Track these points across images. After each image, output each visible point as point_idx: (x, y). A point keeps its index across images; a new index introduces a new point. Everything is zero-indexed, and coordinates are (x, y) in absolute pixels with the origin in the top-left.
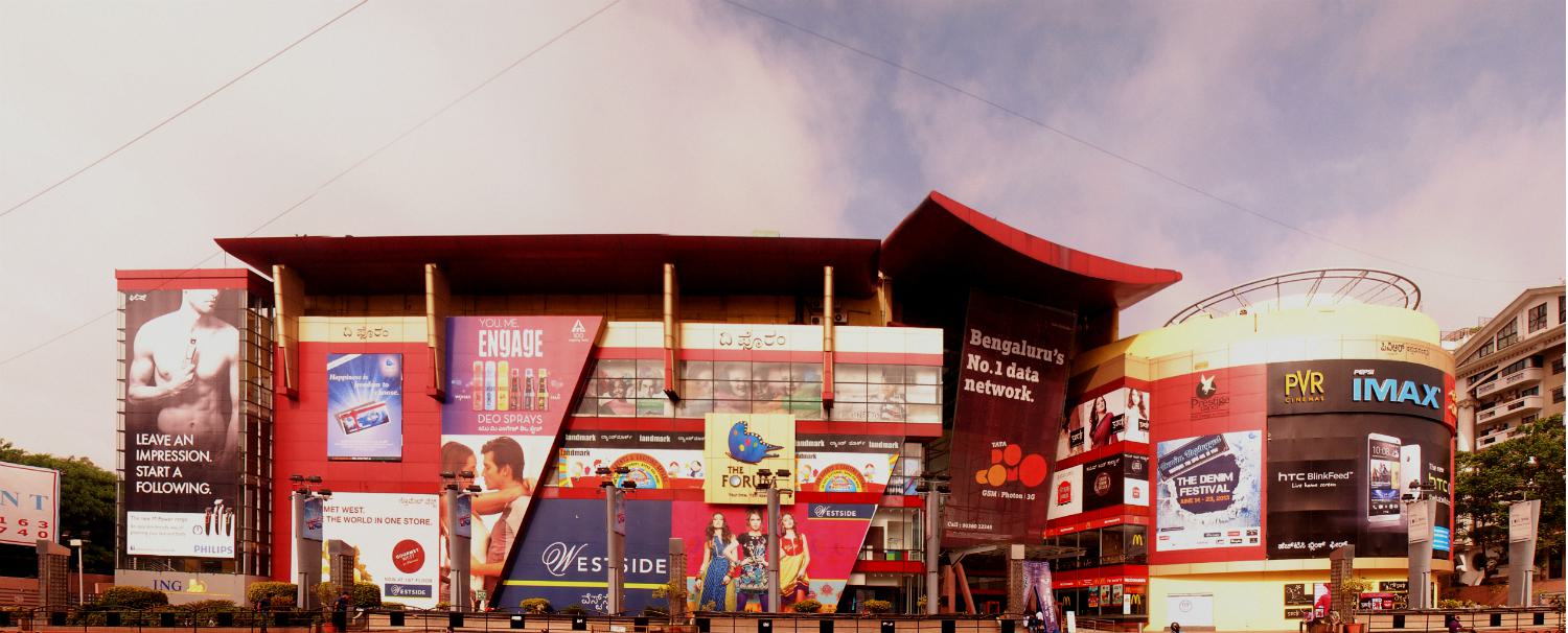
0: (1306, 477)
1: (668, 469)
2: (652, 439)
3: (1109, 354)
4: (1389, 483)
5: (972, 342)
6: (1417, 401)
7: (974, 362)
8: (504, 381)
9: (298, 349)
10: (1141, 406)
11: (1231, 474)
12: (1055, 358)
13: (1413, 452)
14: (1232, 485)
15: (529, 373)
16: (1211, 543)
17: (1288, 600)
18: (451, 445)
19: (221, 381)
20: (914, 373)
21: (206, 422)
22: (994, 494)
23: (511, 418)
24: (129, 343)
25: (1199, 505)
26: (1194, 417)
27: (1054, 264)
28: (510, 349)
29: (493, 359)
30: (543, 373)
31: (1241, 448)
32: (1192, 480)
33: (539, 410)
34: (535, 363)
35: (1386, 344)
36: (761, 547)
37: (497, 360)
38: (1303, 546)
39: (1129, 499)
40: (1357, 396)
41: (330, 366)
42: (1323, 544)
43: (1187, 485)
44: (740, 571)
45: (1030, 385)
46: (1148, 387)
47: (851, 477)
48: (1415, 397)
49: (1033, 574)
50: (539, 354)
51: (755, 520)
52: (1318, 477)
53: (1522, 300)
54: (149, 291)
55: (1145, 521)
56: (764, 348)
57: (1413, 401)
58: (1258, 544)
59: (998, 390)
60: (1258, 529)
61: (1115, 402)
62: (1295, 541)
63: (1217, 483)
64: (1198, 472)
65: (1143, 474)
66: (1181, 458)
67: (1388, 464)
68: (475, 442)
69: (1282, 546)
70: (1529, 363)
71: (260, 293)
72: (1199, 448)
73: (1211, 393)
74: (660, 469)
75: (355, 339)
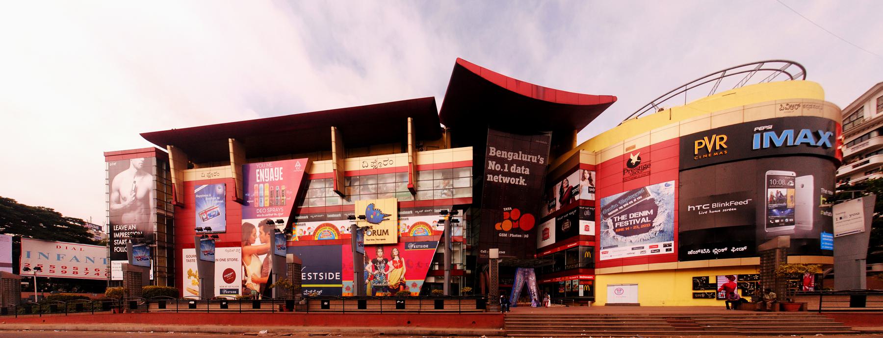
0: (710, 206)
1: (340, 230)
2: (333, 216)
3: (569, 155)
4: (784, 204)
5: (491, 154)
6: (813, 143)
7: (492, 165)
8: (267, 193)
9: (186, 186)
10: (590, 180)
11: (652, 211)
12: (538, 160)
13: (808, 181)
14: (652, 218)
15: (277, 188)
16: (638, 253)
17: (695, 286)
18: (247, 224)
19: (146, 199)
20: (458, 172)
21: (141, 219)
22: (506, 235)
23: (270, 210)
24: (110, 185)
25: (626, 232)
26: (624, 180)
27: (534, 97)
28: (273, 178)
29: (262, 183)
30: (283, 188)
31: (659, 194)
32: (623, 217)
33: (282, 205)
34: (280, 183)
35: (785, 106)
36: (383, 265)
37: (264, 183)
38: (708, 251)
39: (582, 232)
40: (756, 145)
41: (196, 191)
42: (726, 249)
43: (620, 220)
44: (373, 277)
45: (524, 176)
46: (594, 168)
47: (425, 228)
48: (811, 140)
49: (524, 275)
50: (281, 179)
51: (380, 252)
52: (720, 205)
53: (864, 98)
54: (118, 159)
55: (592, 244)
56: (383, 167)
57: (808, 144)
58: (673, 252)
59: (506, 180)
60: (672, 242)
61: (574, 180)
62: (702, 248)
63: (642, 217)
64: (628, 212)
65: (592, 218)
66: (616, 205)
67: (784, 191)
68: (255, 222)
69: (690, 253)
70: (875, 134)
71: (162, 158)
72: (630, 197)
73: (637, 163)
74: (337, 230)
75: (206, 178)
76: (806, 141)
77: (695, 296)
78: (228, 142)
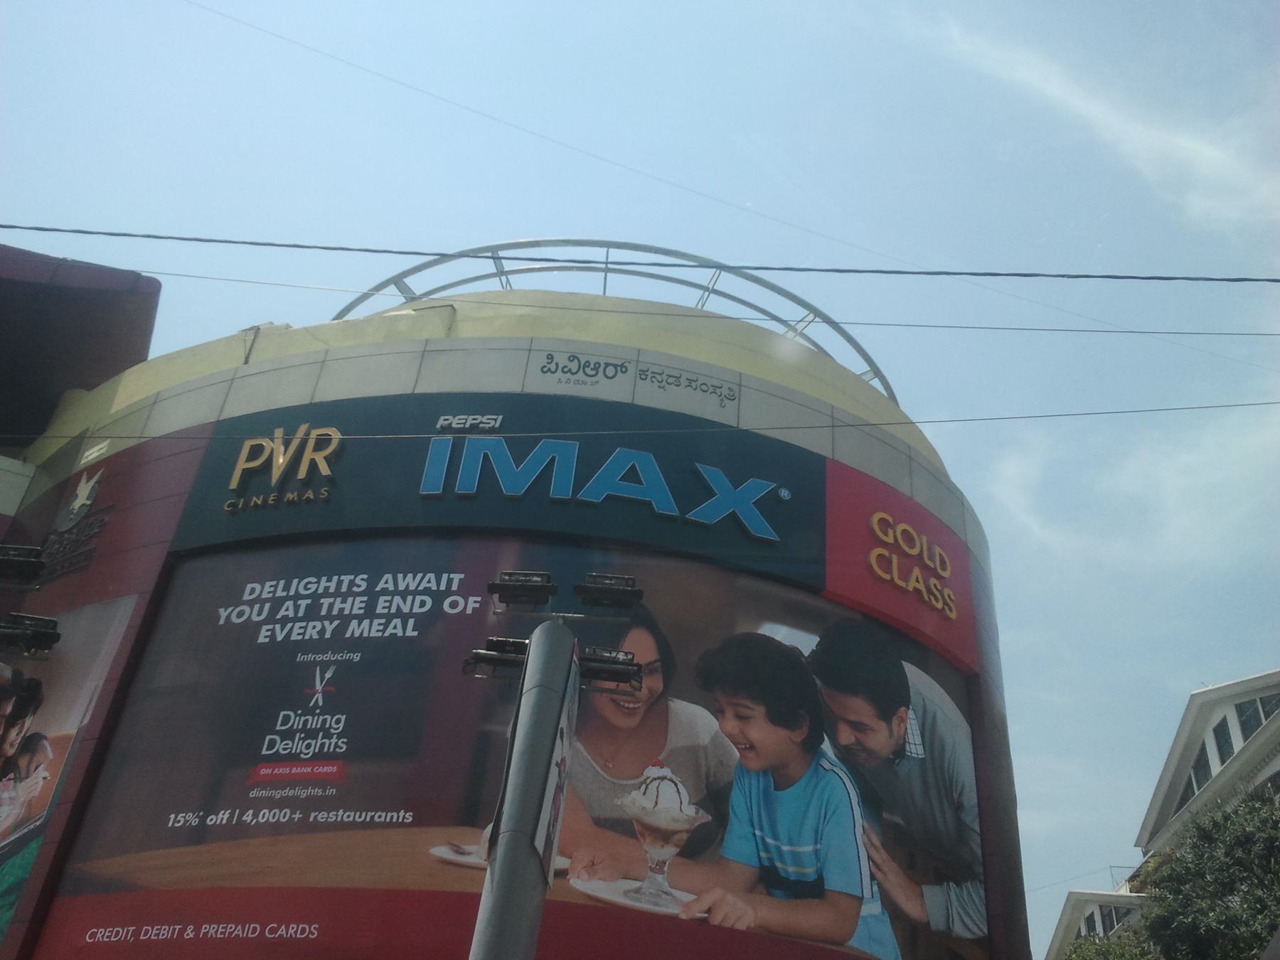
35: (561, 359)
76: (629, 491)
77: (55, 624)
78: (769, 641)
